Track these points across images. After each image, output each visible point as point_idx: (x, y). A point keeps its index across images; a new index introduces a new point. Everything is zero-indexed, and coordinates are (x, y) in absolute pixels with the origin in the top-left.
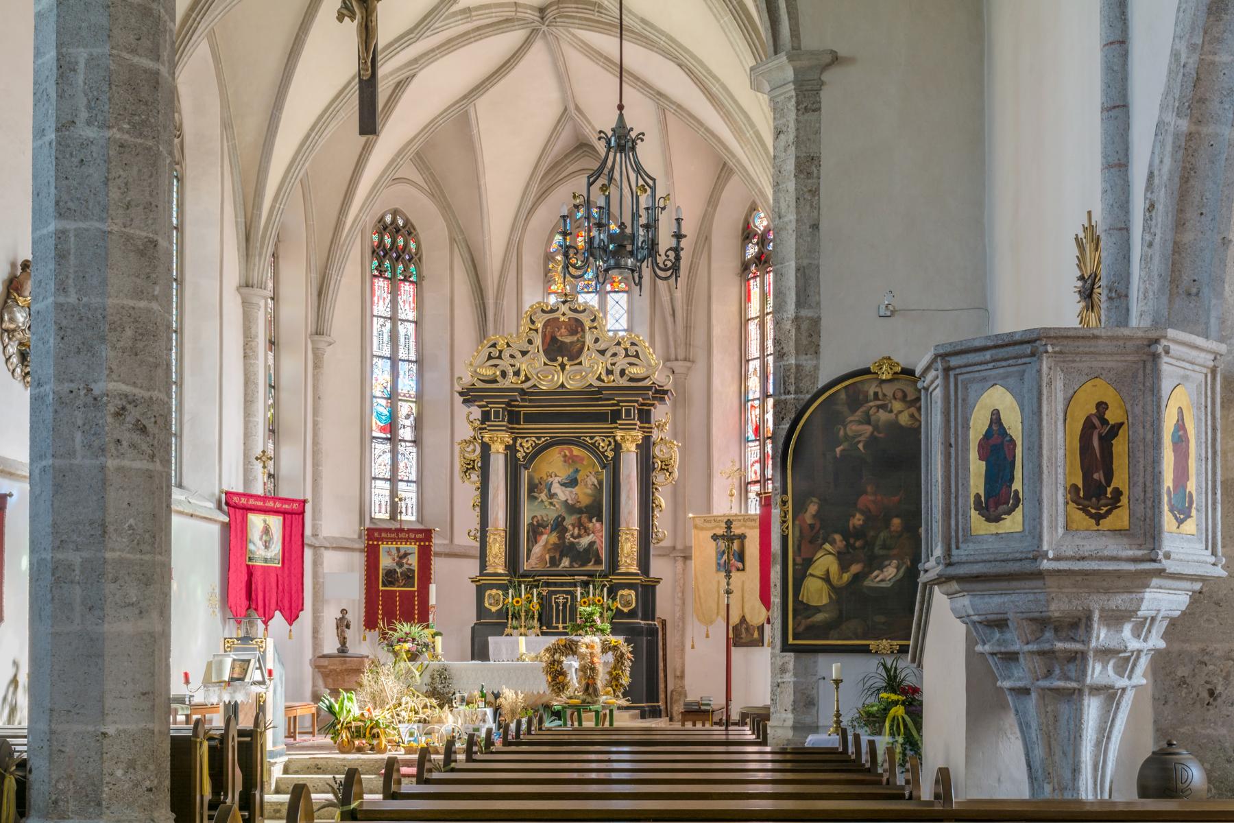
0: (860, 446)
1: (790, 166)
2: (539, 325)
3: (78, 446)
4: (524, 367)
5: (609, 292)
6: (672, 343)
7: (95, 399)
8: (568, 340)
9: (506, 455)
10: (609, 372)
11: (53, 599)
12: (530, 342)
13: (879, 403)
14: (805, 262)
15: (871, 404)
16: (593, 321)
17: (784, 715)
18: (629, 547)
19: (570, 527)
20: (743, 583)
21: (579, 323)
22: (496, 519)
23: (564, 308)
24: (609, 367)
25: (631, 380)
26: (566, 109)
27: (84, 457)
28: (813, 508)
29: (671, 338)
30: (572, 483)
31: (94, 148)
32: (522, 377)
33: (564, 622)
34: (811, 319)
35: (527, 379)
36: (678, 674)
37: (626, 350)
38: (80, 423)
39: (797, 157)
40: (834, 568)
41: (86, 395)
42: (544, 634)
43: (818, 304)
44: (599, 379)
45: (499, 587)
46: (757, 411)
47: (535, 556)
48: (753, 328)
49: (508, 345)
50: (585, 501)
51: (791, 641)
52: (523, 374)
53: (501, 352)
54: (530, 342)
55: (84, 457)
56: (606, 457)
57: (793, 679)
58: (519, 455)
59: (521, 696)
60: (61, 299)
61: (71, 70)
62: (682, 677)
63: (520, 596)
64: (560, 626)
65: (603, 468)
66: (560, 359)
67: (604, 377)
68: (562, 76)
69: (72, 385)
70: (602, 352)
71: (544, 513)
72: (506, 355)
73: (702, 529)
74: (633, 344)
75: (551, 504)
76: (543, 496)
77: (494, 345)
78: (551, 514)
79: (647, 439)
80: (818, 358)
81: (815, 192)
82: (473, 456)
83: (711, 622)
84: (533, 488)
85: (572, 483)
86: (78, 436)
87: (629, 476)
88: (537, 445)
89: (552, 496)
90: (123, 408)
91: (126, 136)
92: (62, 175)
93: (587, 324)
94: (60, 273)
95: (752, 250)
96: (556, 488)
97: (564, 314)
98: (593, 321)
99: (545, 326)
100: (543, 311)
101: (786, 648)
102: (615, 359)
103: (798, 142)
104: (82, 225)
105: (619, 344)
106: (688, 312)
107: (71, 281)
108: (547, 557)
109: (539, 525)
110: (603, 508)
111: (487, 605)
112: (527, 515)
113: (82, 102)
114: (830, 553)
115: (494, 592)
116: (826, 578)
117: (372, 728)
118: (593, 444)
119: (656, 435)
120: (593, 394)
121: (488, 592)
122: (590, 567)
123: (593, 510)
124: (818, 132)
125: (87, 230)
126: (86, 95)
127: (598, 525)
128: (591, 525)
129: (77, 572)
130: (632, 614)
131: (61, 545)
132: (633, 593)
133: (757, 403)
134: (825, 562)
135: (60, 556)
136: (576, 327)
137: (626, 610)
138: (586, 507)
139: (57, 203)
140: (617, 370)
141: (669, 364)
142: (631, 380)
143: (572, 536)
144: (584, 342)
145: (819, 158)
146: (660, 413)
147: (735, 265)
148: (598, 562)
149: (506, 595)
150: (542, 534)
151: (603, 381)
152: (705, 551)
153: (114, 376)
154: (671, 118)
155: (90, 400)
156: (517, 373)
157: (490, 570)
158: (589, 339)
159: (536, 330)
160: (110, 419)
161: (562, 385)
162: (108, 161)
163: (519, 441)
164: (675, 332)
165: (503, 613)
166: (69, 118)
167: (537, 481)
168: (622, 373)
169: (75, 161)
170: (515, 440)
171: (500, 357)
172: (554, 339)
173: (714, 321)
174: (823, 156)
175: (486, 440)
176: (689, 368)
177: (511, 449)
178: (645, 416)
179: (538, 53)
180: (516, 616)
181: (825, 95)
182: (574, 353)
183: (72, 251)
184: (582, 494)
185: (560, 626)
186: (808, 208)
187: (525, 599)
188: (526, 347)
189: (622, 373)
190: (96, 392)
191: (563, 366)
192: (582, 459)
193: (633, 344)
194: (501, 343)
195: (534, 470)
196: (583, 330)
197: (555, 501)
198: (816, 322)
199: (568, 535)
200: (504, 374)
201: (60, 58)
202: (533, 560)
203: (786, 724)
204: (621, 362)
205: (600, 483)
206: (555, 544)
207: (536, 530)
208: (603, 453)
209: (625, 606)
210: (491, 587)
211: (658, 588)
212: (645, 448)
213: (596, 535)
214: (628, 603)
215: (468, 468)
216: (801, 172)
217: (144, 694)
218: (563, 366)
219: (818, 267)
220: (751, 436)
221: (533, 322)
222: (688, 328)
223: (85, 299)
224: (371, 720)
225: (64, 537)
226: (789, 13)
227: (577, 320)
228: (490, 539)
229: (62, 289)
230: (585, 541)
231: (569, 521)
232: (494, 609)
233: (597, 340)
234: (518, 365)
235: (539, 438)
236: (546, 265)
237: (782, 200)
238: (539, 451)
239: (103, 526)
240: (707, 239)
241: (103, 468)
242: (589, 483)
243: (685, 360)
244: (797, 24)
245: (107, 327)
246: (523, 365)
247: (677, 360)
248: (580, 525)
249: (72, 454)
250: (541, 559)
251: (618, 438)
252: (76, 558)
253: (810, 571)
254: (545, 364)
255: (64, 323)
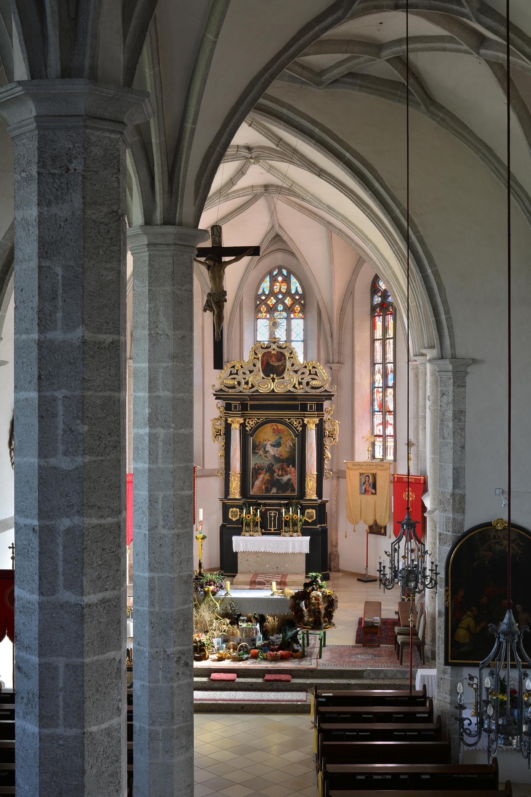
0: (486, 562)
1: (450, 414)
2: (260, 356)
3: (160, 678)
4: (250, 379)
5: (292, 319)
6: (330, 352)
7: (168, 656)
8: (276, 364)
9: (240, 430)
10: (300, 383)
11: (149, 747)
12: (254, 365)
13: (496, 540)
14: (458, 465)
15: (492, 541)
16: (291, 353)
17: (445, 695)
18: (311, 484)
19: (277, 470)
20: (375, 502)
21: (283, 355)
22: (235, 467)
23: (274, 346)
24: (300, 380)
25: (313, 388)
26: (273, 227)
27: (163, 682)
28: (461, 594)
29: (330, 350)
30: (277, 445)
31: (166, 539)
32: (250, 386)
33: (274, 527)
34: (461, 495)
35: (253, 386)
36: (334, 544)
37: (310, 370)
38: (161, 667)
39: (454, 411)
40: (472, 624)
41: (164, 654)
42: (263, 534)
43: (464, 487)
44: (294, 387)
45: (236, 507)
46: (381, 394)
47: (257, 486)
48: (378, 345)
49: (242, 367)
50: (285, 455)
51: (450, 661)
52: (250, 383)
53: (237, 370)
54: (254, 365)
55: (163, 682)
56: (298, 430)
57: (450, 678)
58: (247, 429)
59: (276, 619)
60: (152, 610)
61: (155, 502)
62: (336, 546)
63: (250, 513)
64: (272, 529)
65: (296, 436)
66: (272, 375)
67: (297, 386)
68: (273, 212)
69: (157, 649)
70: (296, 372)
71: (261, 462)
72: (240, 372)
73: (352, 469)
74: (314, 367)
75: (266, 456)
76: (261, 452)
77: (233, 367)
78: (265, 462)
79: (321, 421)
80: (464, 515)
81: (463, 429)
82: (220, 427)
83: (357, 523)
84: (255, 447)
85: (277, 445)
86: (160, 673)
87: (311, 444)
88: (257, 423)
89: (266, 452)
90: (180, 658)
91: (180, 530)
92: (152, 552)
93: (287, 355)
94: (151, 597)
95: (377, 300)
96: (269, 448)
97: (274, 350)
98: (291, 353)
99: (263, 356)
100: (262, 348)
101: (446, 663)
102: (303, 376)
103: (454, 402)
104: (161, 575)
105: (306, 367)
106: (340, 335)
107: (156, 601)
108: (264, 487)
109: (259, 469)
110: (297, 458)
111: (230, 517)
112: (253, 462)
113: (160, 517)
114: (470, 616)
115: (234, 509)
116: (468, 629)
117: (200, 646)
118: (290, 423)
119: (326, 417)
120: (290, 396)
121: (231, 509)
122: (288, 494)
123: (290, 461)
124: (464, 398)
125: (163, 577)
126: (162, 514)
127: (293, 469)
128: (289, 469)
129: (161, 735)
130: (314, 523)
131: (153, 723)
132: (314, 511)
133: (380, 390)
134: (468, 621)
135: (153, 728)
136: (281, 356)
137: (310, 521)
138: (286, 459)
139: (149, 565)
140: (304, 382)
141: (329, 365)
142: (313, 388)
143: (278, 475)
144: (285, 366)
145: (465, 411)
146: (326, 404)
147: (368, 308)
148: (293, 490)
149: (241, 512)
150: (261, 474)
151: (296, 388)
152: (353, 480)
153: (176, 644)
154: (334, 236)
155: (166, 656)
156: (247, 383)
157: (231, 497)
158: (288, 364)
159: (258, 359)
160: (175, 665)
161: (273, 390)
162: (173, 545)
163: (247, 420)
164: (332, 346)
165: (240, 521)
166: (155, 524)
167: (257, 443)
168: (308, 384)
169: (158, 545)
170: (245, 420)
171: (237, 374)
172: (268, 364)
173: (356, 342)
174: (467, 411)
175: (229, 422)
176: (340, 367)
177: (243, 426)
178: (320, 408)
179: (261, 204)
180: (248, 525)
181: (468, 379)
182: (280, 372)
183: (157, 587)
184: (283, 451)
185: (272, 529)
186: (459, 437)
187: (251, 514)
188: (252, 368)
189: (308, 384)
190: (168, 653)
191: (273, 380)
192: (284, 431)
193: (314, 367)
194: (238, 366)
195: (256, 437)
196: (285, 359)
197: (268, 455)
198: (463, 497)
199: (275, 475)
200: (239, 383)
201: (150, 496)
202: (255, 489)
203: (446, 700)
204: (307, 378)
205: (294, 445)
206: (268, 480)
207: (257, 471)
208: (296, 428)
209: (309, 519)
210: (233, 506)
211: (327, 504)
212: (320, 428)
213: (291, 475)
214: (312, 517)
215: (217, 434)
216: (456, 418)
217: (188, 786)
218: (273, 380)
219: (464, 468)
220: (376, 408)
221: (256, 354)
222: (340, 344)
223: (163, 609)
224: (200, 641)
225: (155, 719)
226: (450, 336)
227: (281, 353)
228: (232, 478)
229: (152, 604)
230: (285, 478)
231: (276, 467)
232: (234, 519)
233: (293, 365)
234: (247, 378)
235: (259, 419)
236: (256, 302)
237: (445, 430)
238: (259, 426)
239: (172, 714)
240: (352, 293)
241: (172, 687)
242: (288, 445)
243: (338, 363)
244: (454, 341)
245: (173, 622)
246: (251, 378)
247: (333, 363)
248: (282, 469)
249: (157, 681)
250: (260, 488)
251: (305, 422)
252: (159, 729)
253: (460, 625)
254: (263, 378)
255: (153, 620)
